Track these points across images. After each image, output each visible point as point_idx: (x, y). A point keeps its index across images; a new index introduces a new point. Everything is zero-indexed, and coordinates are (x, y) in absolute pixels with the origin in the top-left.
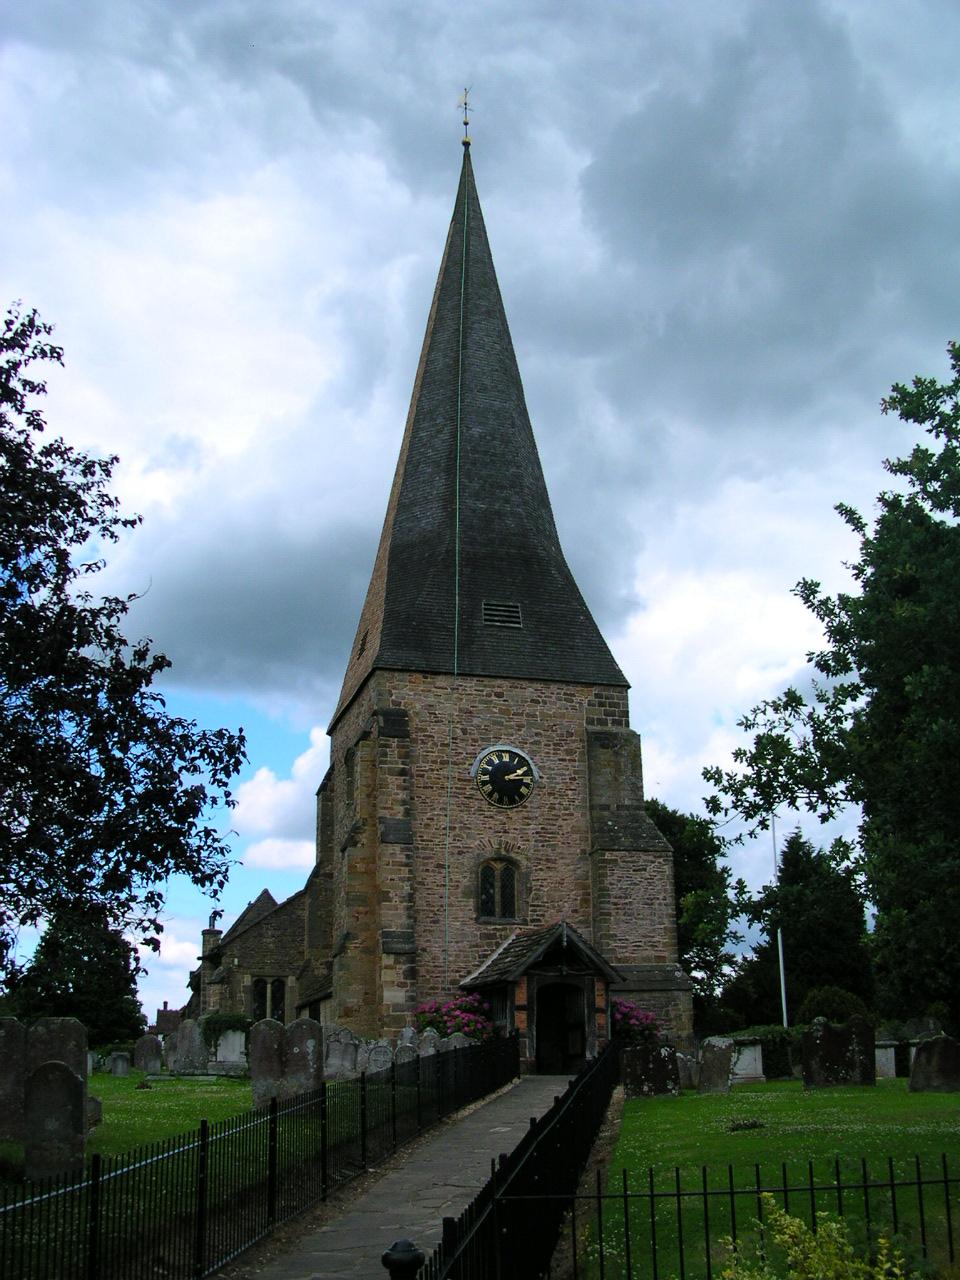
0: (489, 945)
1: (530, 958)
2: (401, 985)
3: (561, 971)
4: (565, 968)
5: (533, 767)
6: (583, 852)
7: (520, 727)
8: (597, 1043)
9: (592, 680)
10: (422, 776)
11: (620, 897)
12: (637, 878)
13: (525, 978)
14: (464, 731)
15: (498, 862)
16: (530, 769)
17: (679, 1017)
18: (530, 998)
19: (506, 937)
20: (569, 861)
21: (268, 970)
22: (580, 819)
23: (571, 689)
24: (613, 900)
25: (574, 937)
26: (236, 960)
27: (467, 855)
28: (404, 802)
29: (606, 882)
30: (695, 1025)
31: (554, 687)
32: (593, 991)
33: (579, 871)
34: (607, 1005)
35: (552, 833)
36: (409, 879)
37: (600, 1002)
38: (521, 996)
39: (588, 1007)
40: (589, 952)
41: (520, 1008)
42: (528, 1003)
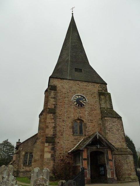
0: (76, 141)
1: (87, 142)
2: (50, 152)
3: (97, 147)
4: (98, 146)
5: (86, 99)
7: (83, 91)
9: (99, 82)
10: (60, 100)
11: (110, 129)
12: (114, 124)
13: (86, 149)
14: (70, 91)
16: (86, 99)
17: (130, 162)
18: (88, 156)
19: (81, 140)
21: (29, 151)
22: (99, 111)
23: (94, 84)
25: (100, 136)
26: (21, 148)
28: (54, 105)
30: (135, 166)
31: (90, 83)
36: (54, 123)
37: (110, 157)
38: (85, 155)
39: (107, 159)
40: (105, 141)
41: (85, 159)
42: (87, 157)
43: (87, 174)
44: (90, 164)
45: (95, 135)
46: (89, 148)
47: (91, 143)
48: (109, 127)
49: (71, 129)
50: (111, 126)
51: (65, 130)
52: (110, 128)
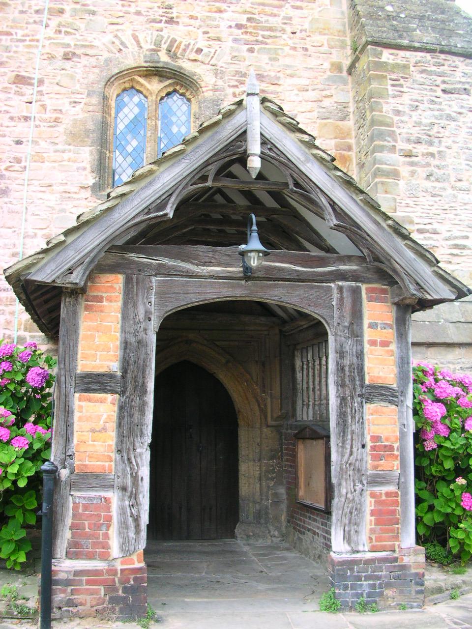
6: (337, 67)
8: (369, 504)
11: (418, 142)
13: (118, 281)
15: (155, 80)
20: (307, 82)
24: (401, 145)
25: (289, 145)
27: (84, 61)
29: (385, 108)
32: (355, 331)
33: (327, 103)
34: (403, 375)
35: (270, 29)
39: (341, 385)
40: (341, 196)
43: (109, 519)
44: (149, 430)
45: (228, 131)
46: (140, 268)
47: (170, 211)
48: (406, 128)
49: (82, 143)
50: (427, 117)
51: (27, 150)
52: (416, 132)
